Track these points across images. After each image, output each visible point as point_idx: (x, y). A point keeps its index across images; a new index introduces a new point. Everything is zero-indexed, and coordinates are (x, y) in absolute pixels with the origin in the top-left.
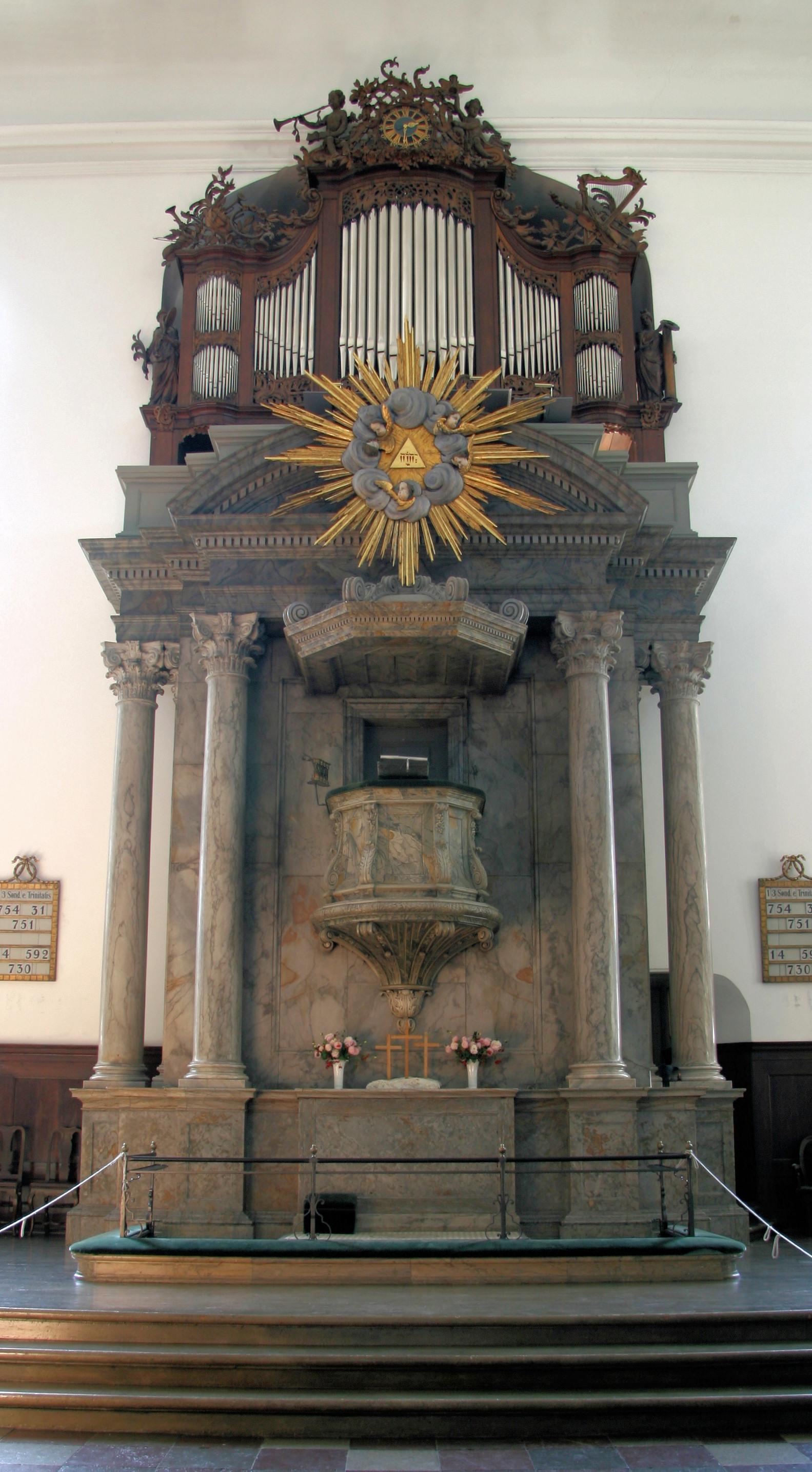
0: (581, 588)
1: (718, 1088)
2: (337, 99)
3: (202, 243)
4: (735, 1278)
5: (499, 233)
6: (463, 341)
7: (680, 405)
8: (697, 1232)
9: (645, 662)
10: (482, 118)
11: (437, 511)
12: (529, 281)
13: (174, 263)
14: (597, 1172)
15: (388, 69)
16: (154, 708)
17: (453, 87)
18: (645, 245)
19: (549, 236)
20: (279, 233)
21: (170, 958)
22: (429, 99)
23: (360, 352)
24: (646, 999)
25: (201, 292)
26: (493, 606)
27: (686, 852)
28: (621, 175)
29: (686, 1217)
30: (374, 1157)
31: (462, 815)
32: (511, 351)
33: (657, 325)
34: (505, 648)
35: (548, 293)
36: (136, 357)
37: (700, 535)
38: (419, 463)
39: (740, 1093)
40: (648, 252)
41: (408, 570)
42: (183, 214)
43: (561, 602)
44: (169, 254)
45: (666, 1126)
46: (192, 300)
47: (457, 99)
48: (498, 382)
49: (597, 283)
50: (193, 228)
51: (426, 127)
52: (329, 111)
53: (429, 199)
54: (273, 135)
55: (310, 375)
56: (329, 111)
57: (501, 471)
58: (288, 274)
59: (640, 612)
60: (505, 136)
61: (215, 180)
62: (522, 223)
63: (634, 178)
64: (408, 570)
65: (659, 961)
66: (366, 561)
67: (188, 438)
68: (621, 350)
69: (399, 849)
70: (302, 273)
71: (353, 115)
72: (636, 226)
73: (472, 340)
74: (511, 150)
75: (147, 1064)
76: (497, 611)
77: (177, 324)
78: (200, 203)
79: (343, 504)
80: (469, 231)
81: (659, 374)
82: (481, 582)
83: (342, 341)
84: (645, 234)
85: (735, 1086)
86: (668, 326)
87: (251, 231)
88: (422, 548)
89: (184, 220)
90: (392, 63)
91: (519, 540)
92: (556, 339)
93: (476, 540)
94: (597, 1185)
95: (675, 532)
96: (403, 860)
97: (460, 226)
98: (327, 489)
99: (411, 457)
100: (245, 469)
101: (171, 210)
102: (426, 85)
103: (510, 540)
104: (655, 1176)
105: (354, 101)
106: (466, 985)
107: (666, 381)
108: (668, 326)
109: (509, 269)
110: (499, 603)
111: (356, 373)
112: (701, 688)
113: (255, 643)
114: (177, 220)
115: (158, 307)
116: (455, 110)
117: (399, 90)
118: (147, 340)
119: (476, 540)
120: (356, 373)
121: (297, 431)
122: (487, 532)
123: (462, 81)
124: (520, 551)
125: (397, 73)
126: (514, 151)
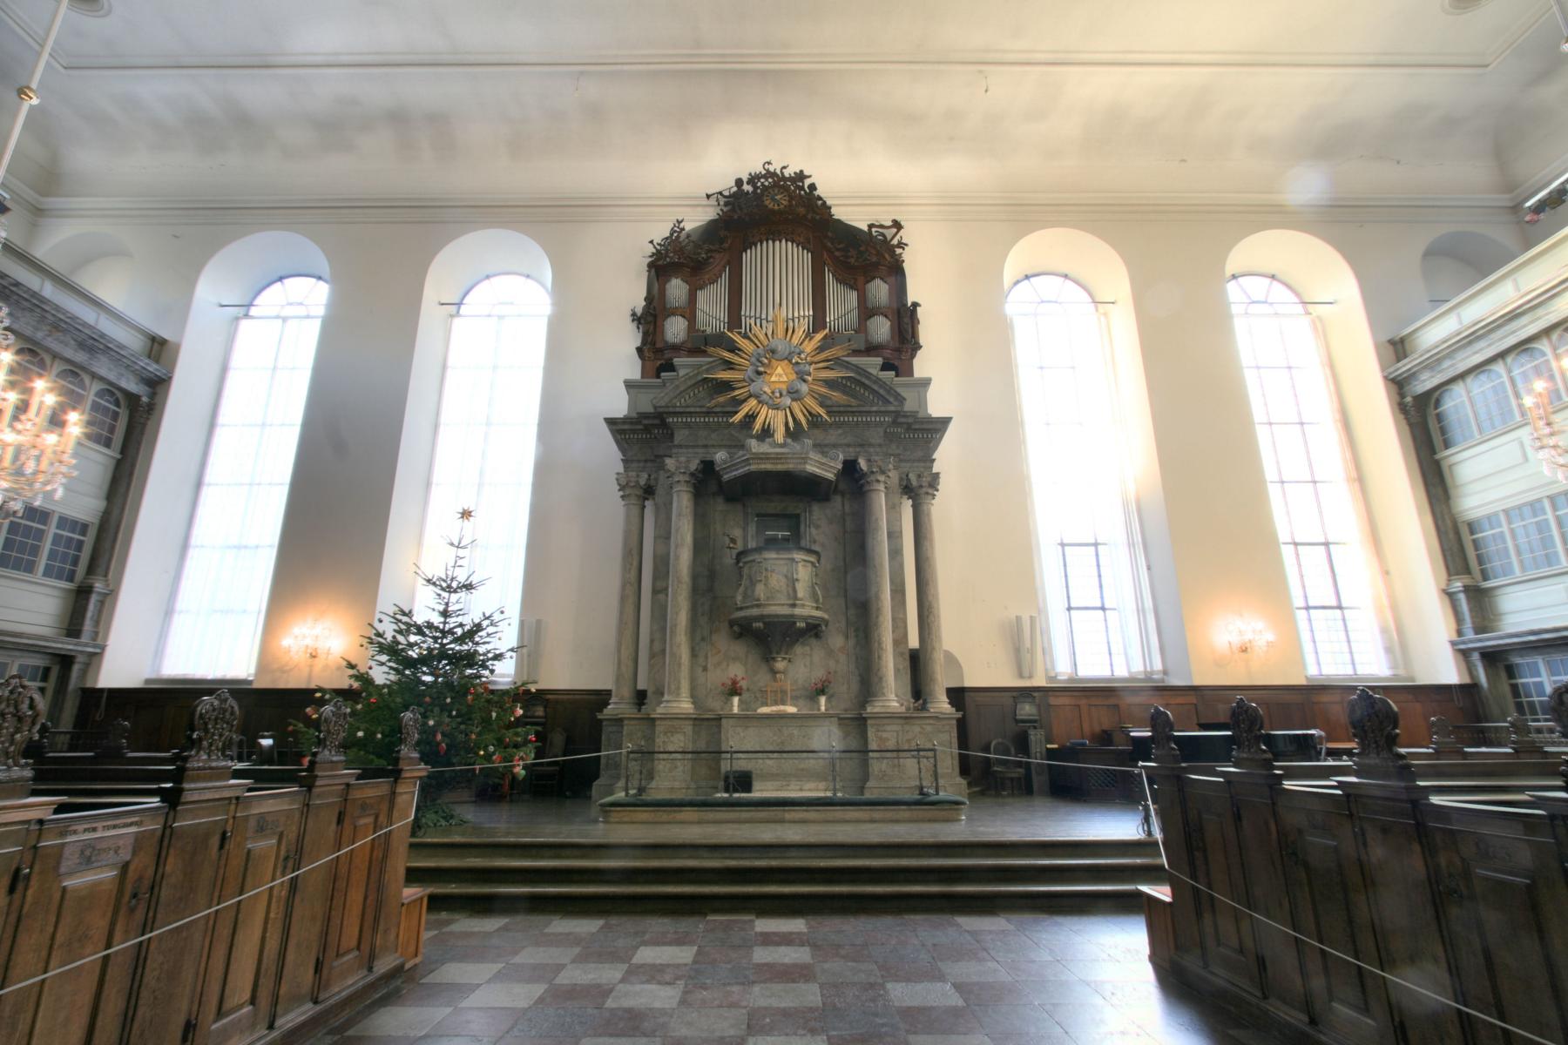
0: (870, 445)
1: (944, 711)
2: (739, 182)
3: (668, 260)
4: (963, 820)
5: (825, 256)
6: (807, 314)
7: (921, 347)
8: (941, 793)
9: (905, 483)
10: (816, 193)
11: (794, 404)
12: (839, 281)
13: (653, 270)
14: (883, 758)
15: (766, 166)
16: (644, 507)
17: (801, 176)
18: (903, 261)
19: (852, 257)
20: (709, 255)
21: (652, 641)
22: (789, 183)
23: (753, 319)
24: (907, 663)
25: (668, 286)
26: (823, 453)
27: (927, 584)
28: (890, 224)
29: (934, 785)
30: (762, 749)
31: (809, 564)
32: (832, 319)
33: (909, 304)
34: (830, 476)
35: (852, 288)
36: (633, 321)
37: (933, 416)
38: (785, 379)
39: (959, 715)
40: (904, 264)
41: (780, 436)
42: (658, 244)
43: (859, 452)
44: (650, 265)
45: (920, 733)
46: (663, 292)
47: (803, 183)
48: (825, 337)
49: (878, 282)
50: (663, 252)
51: (787, 198)
52: (735, 189)
53: (788, 237)
54: (705, 202)
55: (726, 331)
56: (735, 189)
57: (830, 384)
58: (714, 277)
59: (902, 457)
60: (829, 202)
61: (675, 226)
62: (838, 250)
63: (897, 225)
64: (780, 436)
65: (914, 642)
66: (757, 431)
67: (661, 365)
68: (890, 317)
69: (775, 582)
70: (721, 277)
71: (748, 191)
72: (898, 251)
73: (811, 313)
74: (832, 210)
75: (638, 699)
76: (826, 457)
77: (655, 303)
78: (667, 238)
79: (745, 400)
80: (810, 254)
81: (910, 330)
82: (818, 442)
83: (743, 313)
84: (903, 255)
85: (957, 711)
86: (915, 305)
87: (694, 254)
88: (787, 424)
89: (658, 247)
90: (769, 163)
91: (837, 419)
92: (856, 313)
93: (815, 420)
94: (884, 765)
95: (921, 415)
96: (777, 588)
97: (805, 251)
98: (737, 392)
99: (780, 375)
100: (693, 382)
101: (651, 242)
102: (787, 175)
103: (833, 419)
104: (915, 760)
105: (748, 183)
106: (811, 655)
107: (914, 335)
108: (915, 305)
109: (831, 275)
110: (827, 452)
111: (750, 330)
112: (934, 496)
113: (700, 472)
114: (655, 247)
115: (644, 294)
116: (802, 188)
117: (773, 178)
118: (639, 311)
119: (815, 420)
120: (750, 330)
121: (720, 361)
122: (820, 415)
123: (806, 173)
124: (838, 425)
125: (772, 169)
126: (833, 211)
